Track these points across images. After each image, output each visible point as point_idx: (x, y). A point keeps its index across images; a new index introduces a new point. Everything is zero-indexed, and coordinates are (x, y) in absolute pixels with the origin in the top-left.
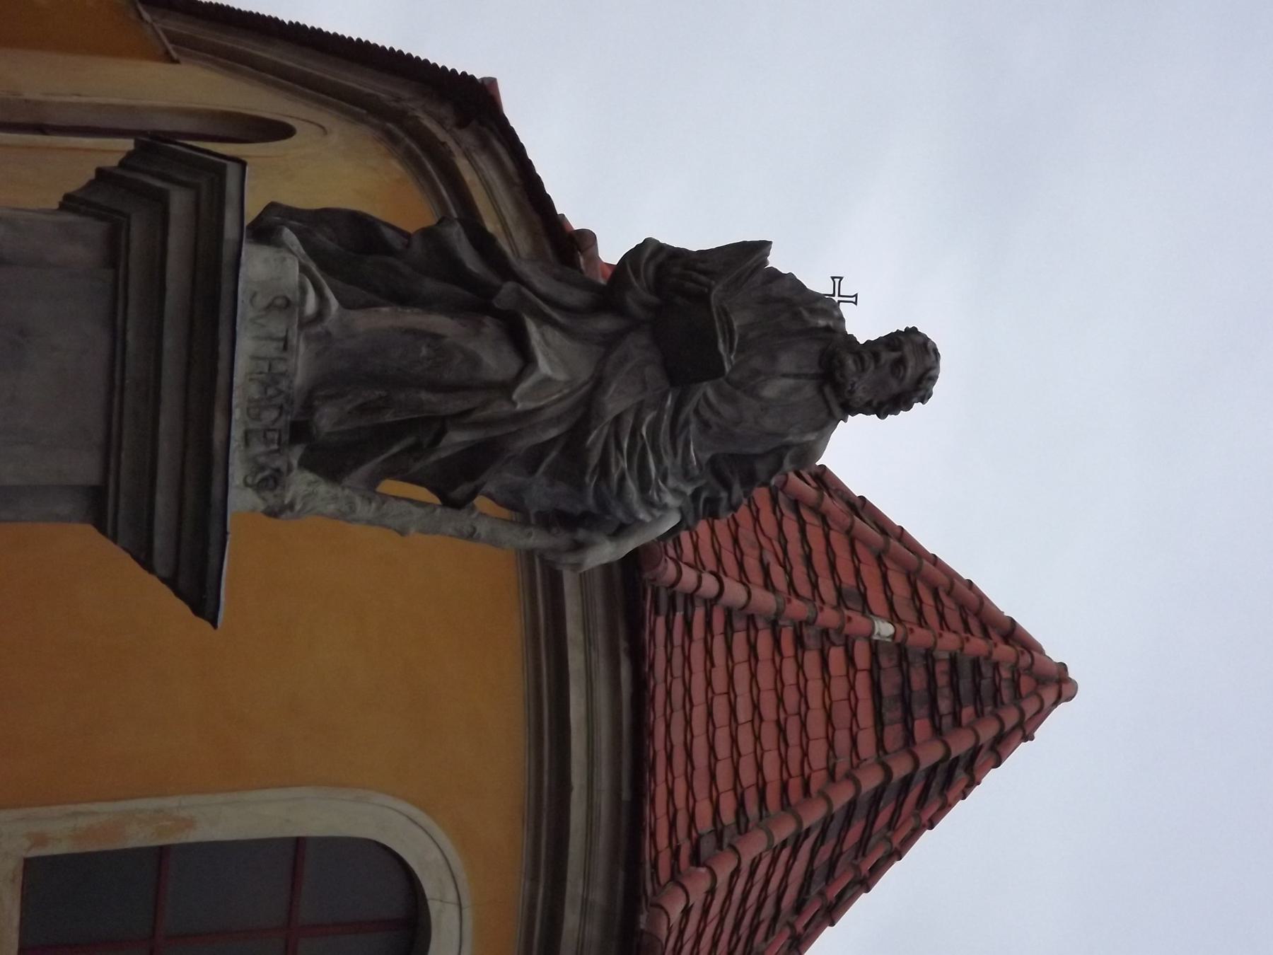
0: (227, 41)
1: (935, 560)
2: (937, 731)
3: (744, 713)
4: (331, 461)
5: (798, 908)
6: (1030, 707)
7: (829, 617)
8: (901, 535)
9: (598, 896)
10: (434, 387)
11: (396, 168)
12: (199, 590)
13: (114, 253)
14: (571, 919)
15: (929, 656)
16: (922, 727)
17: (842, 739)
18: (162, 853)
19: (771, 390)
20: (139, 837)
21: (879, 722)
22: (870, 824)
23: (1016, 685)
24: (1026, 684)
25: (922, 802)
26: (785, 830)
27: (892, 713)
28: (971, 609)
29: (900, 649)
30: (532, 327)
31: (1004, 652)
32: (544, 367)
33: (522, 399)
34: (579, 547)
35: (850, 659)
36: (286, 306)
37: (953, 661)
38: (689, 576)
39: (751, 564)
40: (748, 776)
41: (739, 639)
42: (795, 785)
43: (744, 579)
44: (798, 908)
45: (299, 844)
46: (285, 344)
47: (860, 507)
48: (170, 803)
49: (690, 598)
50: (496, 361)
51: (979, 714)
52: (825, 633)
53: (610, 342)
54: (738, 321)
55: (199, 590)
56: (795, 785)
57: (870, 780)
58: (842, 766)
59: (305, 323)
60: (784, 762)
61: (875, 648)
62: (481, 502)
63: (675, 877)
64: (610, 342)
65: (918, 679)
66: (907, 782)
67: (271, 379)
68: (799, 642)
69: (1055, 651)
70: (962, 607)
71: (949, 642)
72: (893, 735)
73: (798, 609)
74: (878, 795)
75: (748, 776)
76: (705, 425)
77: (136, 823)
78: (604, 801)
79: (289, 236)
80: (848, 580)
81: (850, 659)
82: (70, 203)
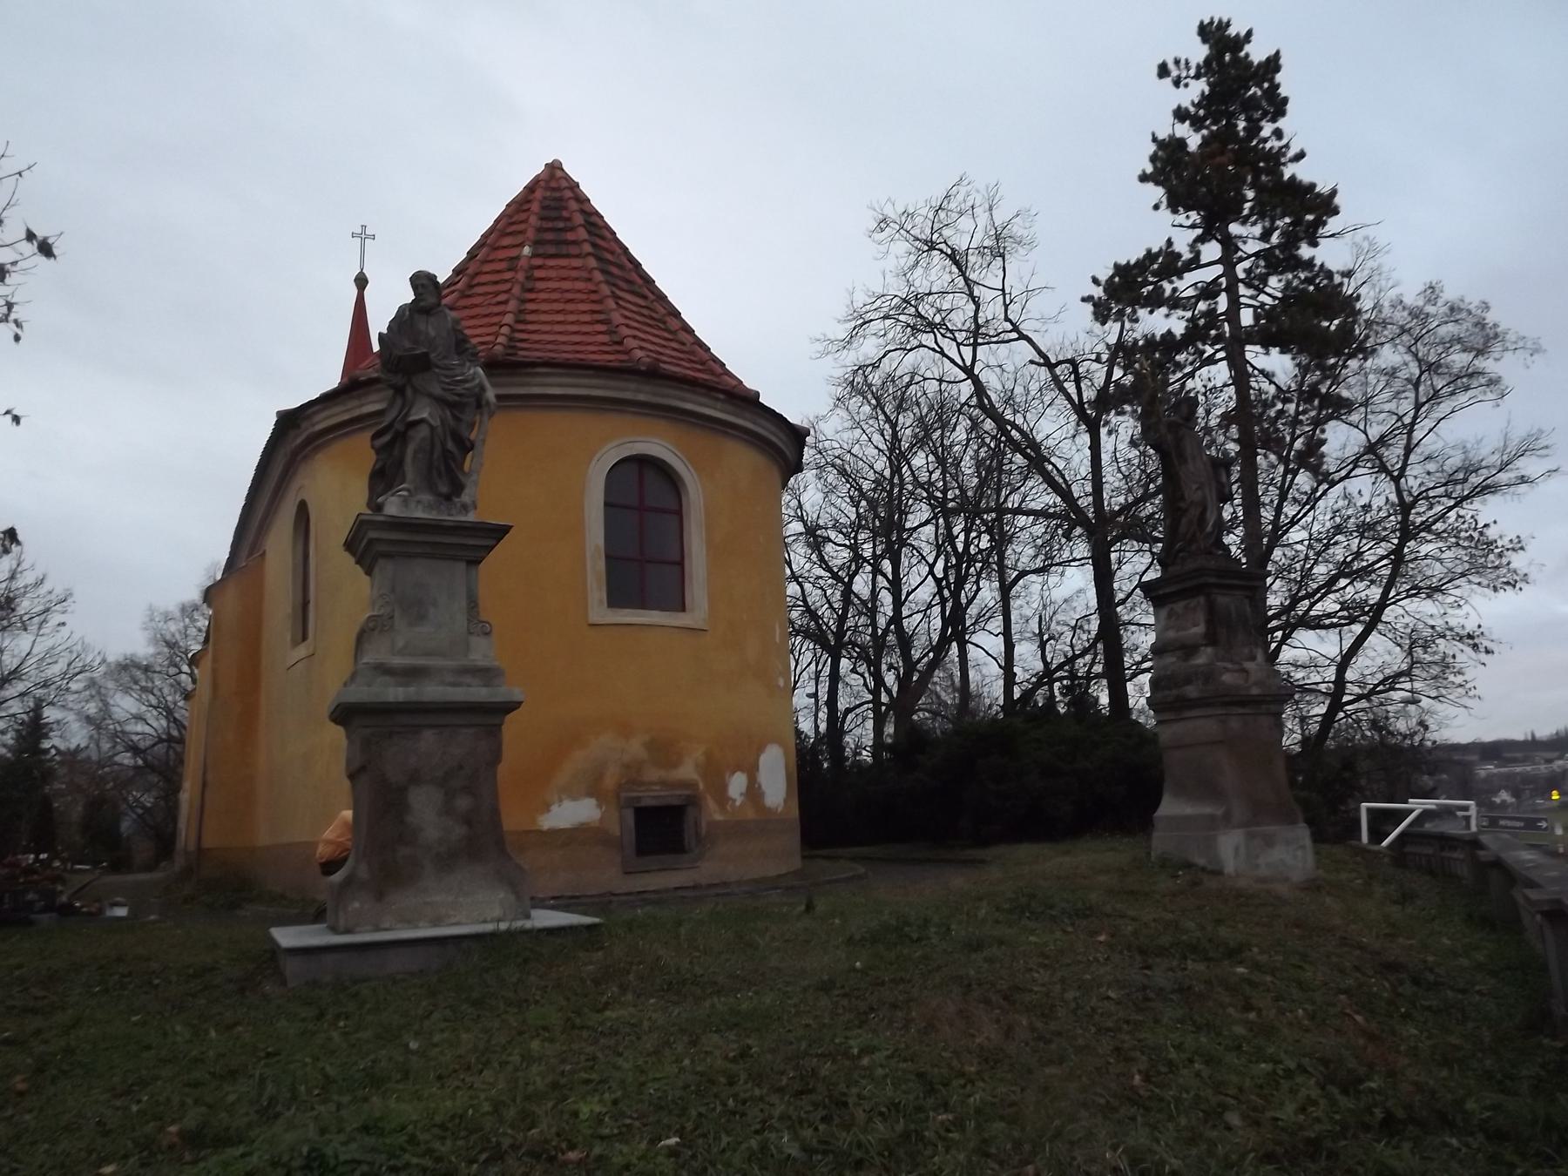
0: (255, 524)
1: (497, 221)
2: (572, 229)
3: (560, 318)
4: (458, 488)
5: (645, 297)
6: (564, 184)
7: (520, 276)
8: (485, 236)
9: (633, 386)
10: (432, 453)
11: (319, 456)
12: (501, 532)
13: (388, 556)
14: (642, 397)
15: (539, 230)
16: (570, 236)
17: (574, 274)
18: (608, 557)
19: (432, 333)
20: (601, 565)
21: (567, 256)
22: (611, 263)
23: (554, 189)
24: (553, 184)
25: (603, 238)
26: (611, 304)
27: (564, 250)
28: (519, 207)
29: (536, 243)
30: (412, 418)
31: (539, 194)
32: (425, 415)
33: (436, 422)
34: (488, 403)
35: (539, 267)
36: (405, 501)
37: (542, 219)
38: (501, 339)
39: (496, 309)
40: (587, 318)
41: (530, 317)
42: (594, 297)
43: (504, 313)
44: (645, 297)
45: (606, 504)
46: (419, 502)
47: (472, 255)
48: (588, 555)
49: (511, 339)
50: (423, 431)
51: (566, 208)
52: (527, 278)
53: (415, 391)
54: (407, 344)
55: (501, 532)
56: (594, 297)
57: (592, 262)
58: (584, 274)
59: (411, 495)
60: (582, 301)
61: (534, 255)
62: (472, 437)
63: (628, 352)
64: (415, 391)
65: (549, 236)
66: (594, 245)
67: (430, 507)
68: (531, 290)
69: (539, 169)
70: (518, 211)
71: (533, 220)
72: (574, 250)
73: (516, 290)
74: (599, 259)
75: (587, 318)
76: (445, 358)
77: (596, 566)
78: (594, 381)
79: (380, 500)
80: (503, 265)
81: (539, 267)
82: (369, 572)
